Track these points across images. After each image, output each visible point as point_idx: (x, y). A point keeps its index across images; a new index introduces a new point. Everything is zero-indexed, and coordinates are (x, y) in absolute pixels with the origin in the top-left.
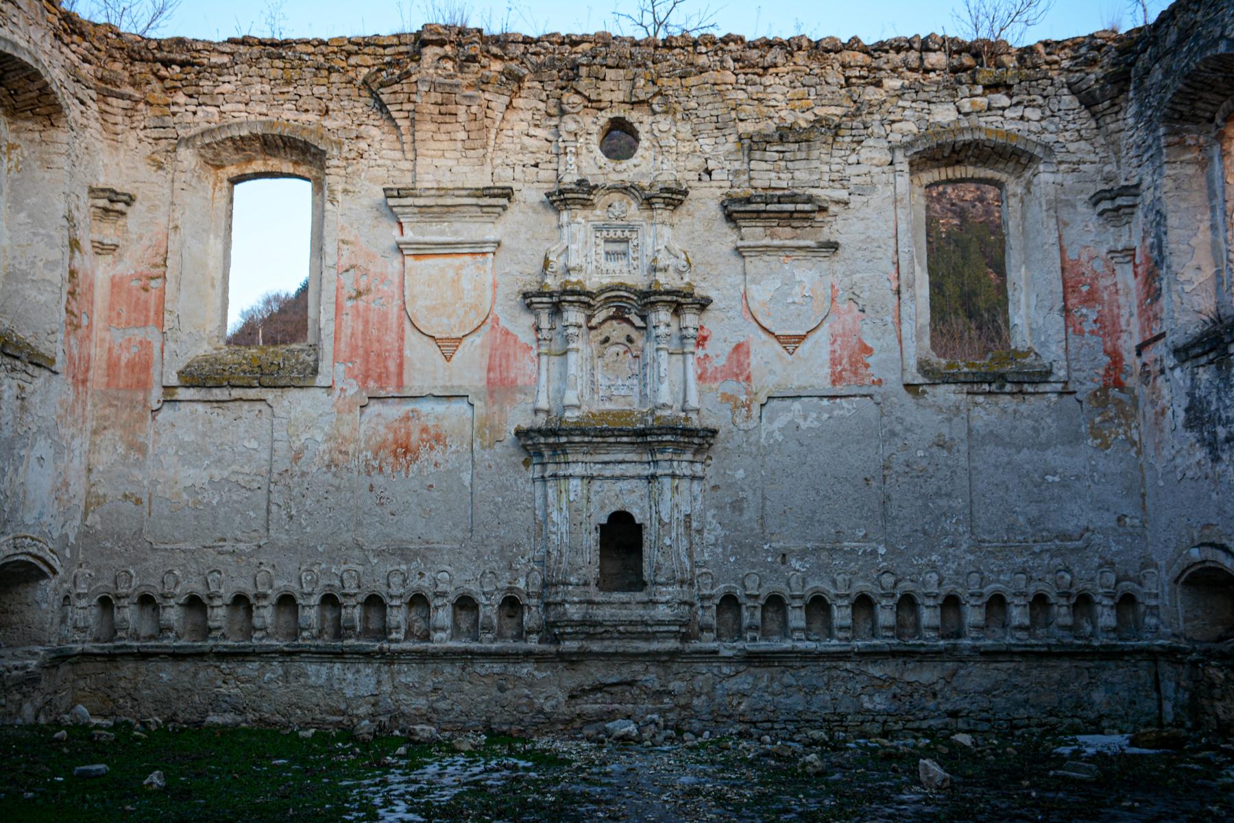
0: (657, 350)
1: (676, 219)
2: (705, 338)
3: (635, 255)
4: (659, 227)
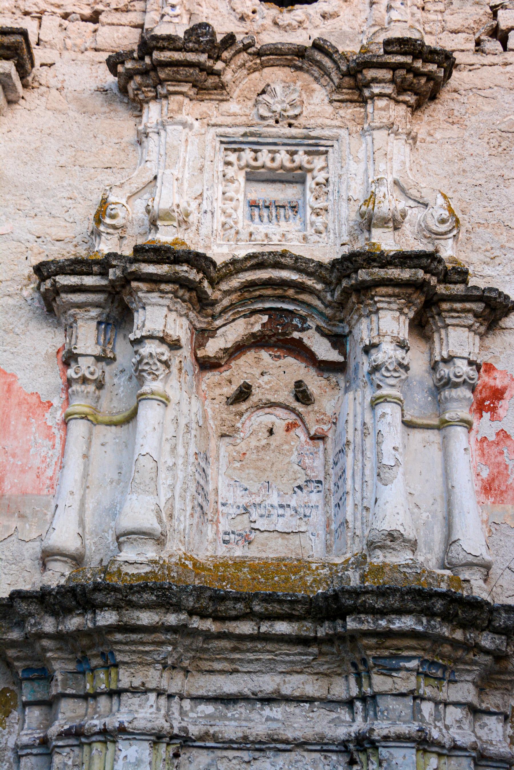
0: (375, 403)
1: (421, 129)
2: (498, 394)
4: (380, 135)
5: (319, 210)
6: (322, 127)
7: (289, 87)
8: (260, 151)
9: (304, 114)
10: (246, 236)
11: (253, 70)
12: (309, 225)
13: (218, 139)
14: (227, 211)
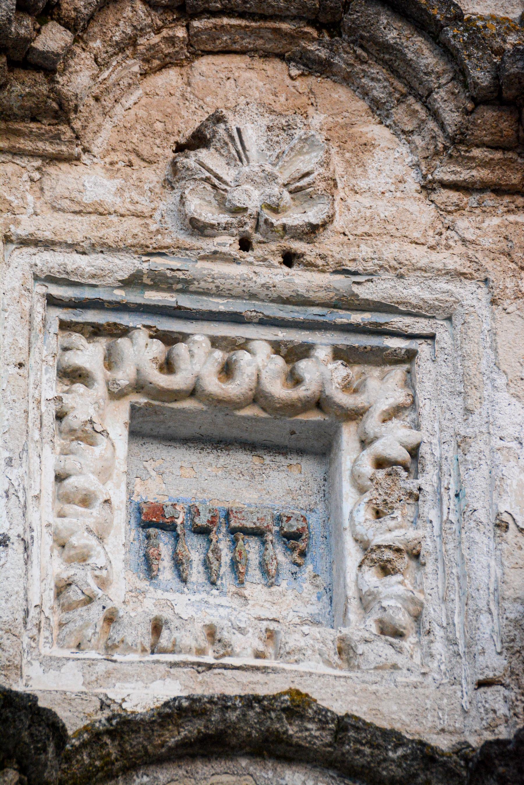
3: (393, 532)
5: (388, 555)
6: (399, 271)
7: (287, 128)
8: (184, 337)
9: (338, 224)
10: (137, 633)
11: (158, 62)
12: (354, 605)
13: (40, 289)
14: (74, 540)
